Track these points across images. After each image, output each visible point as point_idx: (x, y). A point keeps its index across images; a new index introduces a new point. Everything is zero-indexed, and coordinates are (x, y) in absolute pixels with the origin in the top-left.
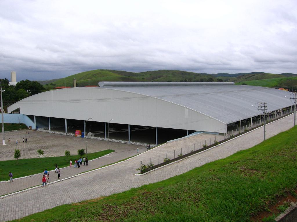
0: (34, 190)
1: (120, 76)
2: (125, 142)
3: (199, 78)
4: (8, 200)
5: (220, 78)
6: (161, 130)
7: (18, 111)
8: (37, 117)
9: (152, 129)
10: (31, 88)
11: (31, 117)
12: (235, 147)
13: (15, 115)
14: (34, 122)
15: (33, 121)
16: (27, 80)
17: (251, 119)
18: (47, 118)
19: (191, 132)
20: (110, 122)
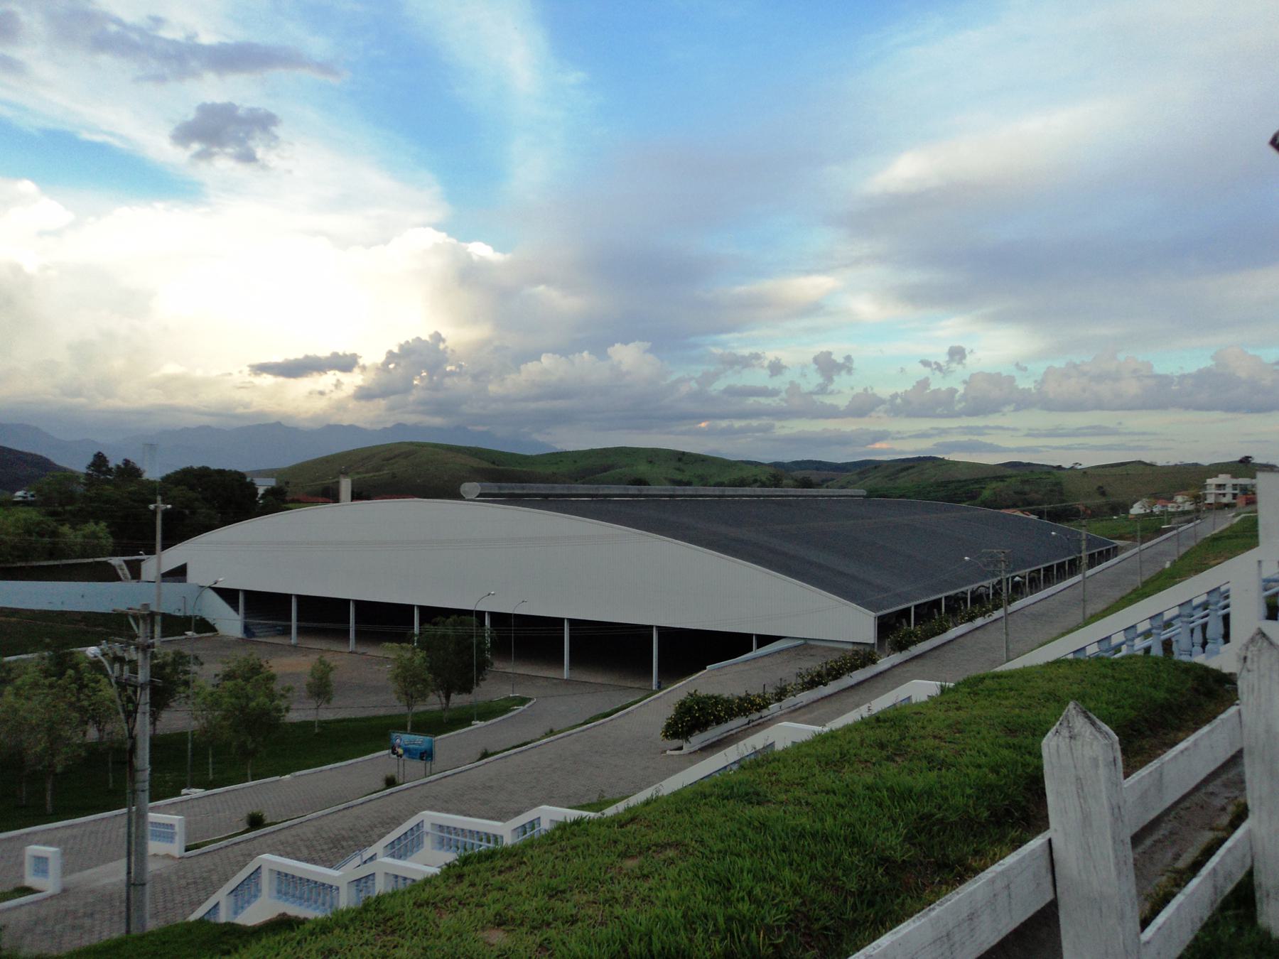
0: (336, 816)
1: (485, 465)
2: (551, 674)
3: (736, 475)
4: (67, 912)
5: (799, 474)
6: (669, 635)
7: (179, 573)
8: (248, 593)
9: (641, 632)
10: (217, 497)
11: (229, 595)
12: (567, 909)
13: (171, 587)
14: (237, 610)
15: (235, 606)
16: (127, 462)
17: (164, 538)
18: (284, 599)
19: (765, 640)
20: (516, 612)
